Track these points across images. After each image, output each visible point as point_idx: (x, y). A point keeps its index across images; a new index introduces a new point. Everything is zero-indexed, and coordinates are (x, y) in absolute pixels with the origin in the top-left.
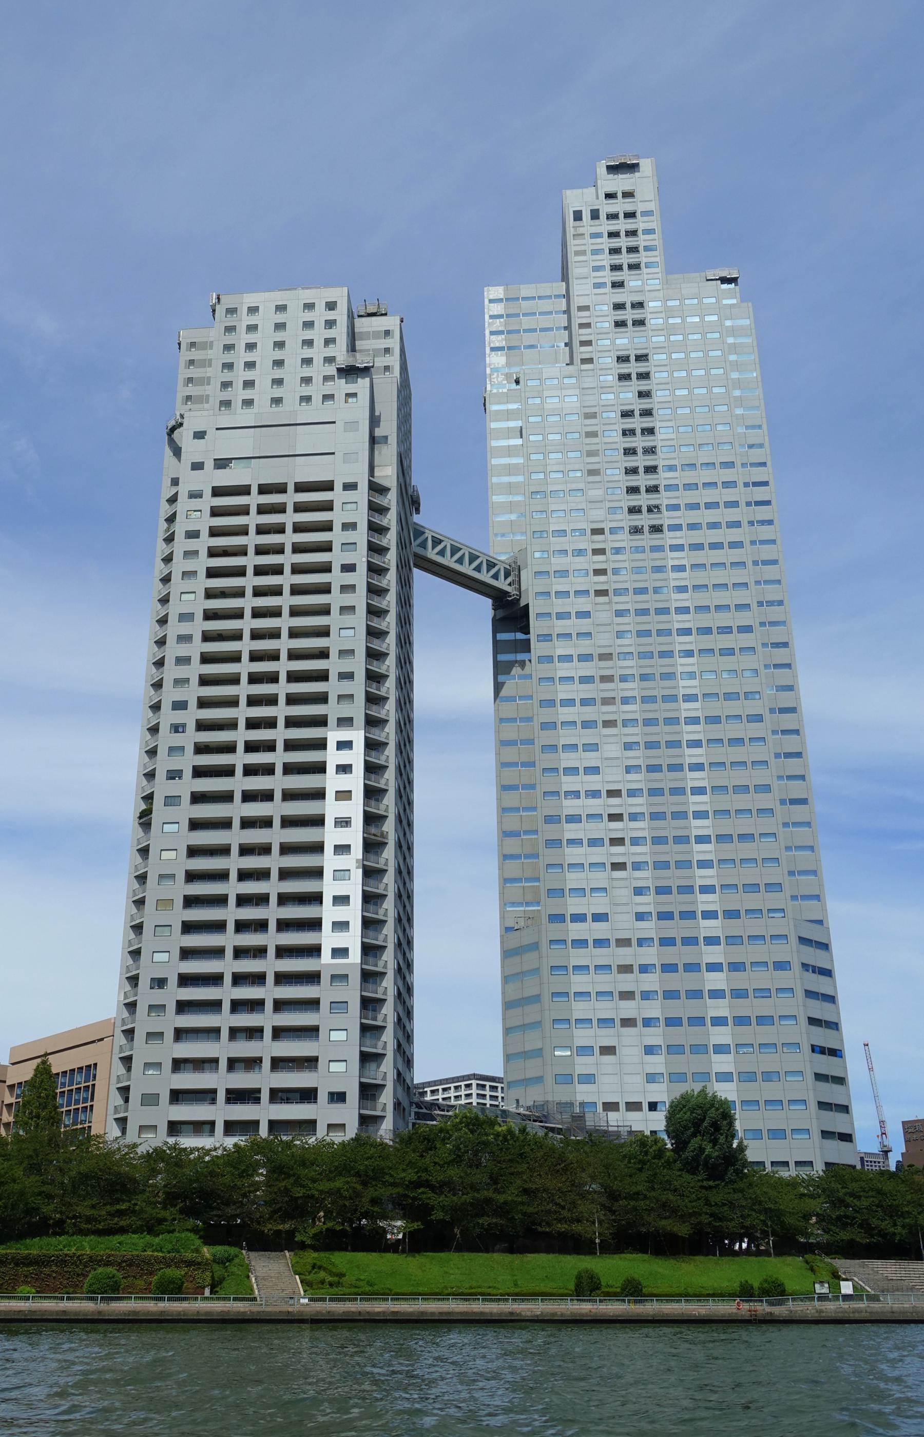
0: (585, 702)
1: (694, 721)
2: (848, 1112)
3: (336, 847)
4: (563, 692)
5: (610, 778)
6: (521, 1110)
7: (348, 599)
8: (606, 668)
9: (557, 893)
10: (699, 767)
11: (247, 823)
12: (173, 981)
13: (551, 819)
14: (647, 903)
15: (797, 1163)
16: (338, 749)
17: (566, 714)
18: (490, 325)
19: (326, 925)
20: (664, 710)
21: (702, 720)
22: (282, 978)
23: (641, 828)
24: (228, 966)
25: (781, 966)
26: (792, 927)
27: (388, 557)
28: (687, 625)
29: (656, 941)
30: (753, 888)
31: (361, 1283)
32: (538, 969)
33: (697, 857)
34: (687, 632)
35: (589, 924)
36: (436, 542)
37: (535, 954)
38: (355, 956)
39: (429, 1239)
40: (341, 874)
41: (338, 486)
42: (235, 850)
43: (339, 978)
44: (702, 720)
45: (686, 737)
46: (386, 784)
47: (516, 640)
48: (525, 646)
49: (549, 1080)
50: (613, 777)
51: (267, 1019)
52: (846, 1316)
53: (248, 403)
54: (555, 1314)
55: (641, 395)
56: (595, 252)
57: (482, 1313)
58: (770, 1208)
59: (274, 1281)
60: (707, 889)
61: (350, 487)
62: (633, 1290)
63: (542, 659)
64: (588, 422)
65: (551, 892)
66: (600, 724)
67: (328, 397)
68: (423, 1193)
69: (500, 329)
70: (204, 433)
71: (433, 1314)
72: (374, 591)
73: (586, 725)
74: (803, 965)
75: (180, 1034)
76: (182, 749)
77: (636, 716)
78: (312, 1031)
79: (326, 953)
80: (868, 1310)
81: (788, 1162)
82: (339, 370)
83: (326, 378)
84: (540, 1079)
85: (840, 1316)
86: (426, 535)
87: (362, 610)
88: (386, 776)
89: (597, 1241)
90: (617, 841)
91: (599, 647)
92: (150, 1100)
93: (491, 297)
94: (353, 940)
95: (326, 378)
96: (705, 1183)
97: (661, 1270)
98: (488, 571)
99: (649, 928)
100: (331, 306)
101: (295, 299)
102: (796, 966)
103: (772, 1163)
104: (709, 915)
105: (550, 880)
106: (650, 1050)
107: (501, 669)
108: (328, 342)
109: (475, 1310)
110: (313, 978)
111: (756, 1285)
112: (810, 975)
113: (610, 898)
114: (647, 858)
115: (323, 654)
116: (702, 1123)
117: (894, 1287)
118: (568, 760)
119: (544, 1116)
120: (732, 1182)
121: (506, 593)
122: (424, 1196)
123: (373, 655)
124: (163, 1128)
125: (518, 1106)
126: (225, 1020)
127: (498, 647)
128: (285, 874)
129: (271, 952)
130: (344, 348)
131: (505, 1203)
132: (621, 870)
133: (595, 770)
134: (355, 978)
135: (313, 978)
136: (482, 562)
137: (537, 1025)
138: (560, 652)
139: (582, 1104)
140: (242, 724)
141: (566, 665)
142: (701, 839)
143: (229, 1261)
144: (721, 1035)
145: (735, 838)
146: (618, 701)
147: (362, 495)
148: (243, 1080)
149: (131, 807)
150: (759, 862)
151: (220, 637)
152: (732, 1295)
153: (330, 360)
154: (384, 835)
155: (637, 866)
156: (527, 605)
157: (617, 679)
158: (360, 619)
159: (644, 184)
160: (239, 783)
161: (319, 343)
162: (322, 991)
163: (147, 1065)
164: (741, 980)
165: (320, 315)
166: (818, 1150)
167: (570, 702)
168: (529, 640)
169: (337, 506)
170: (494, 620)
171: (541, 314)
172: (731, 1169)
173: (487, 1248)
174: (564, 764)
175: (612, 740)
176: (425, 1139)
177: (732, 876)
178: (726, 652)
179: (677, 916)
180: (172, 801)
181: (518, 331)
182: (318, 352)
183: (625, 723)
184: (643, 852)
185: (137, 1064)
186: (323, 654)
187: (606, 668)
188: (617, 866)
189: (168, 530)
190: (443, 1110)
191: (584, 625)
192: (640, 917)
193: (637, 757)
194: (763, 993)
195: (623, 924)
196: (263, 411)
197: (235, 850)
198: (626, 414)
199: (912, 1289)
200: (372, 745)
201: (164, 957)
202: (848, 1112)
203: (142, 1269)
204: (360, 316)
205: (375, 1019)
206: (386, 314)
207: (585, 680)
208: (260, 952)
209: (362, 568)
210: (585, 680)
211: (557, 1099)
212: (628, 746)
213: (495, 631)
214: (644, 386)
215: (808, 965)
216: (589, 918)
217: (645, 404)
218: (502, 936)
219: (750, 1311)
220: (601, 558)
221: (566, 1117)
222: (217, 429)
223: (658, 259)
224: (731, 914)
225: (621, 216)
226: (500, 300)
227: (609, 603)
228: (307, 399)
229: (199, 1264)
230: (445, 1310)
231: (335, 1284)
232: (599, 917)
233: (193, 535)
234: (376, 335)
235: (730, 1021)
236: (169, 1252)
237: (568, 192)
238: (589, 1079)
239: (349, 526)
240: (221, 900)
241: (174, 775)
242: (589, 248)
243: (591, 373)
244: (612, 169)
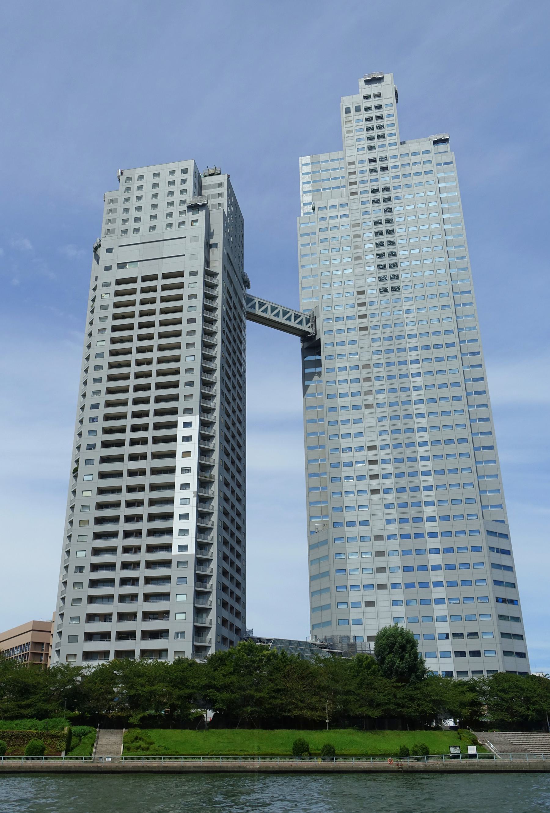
0: (354, 394)
1: (421, 402)
2: (522, 639)
3: (182, 485)
4: (341, 389)
5: (370, 439)
6: (318, 642)
7: (191, 339)
8: (366, 373)
9: (338, 509)
10: (424, 429)
11: (132, 473)
12: (88, 568)
13: (335, 465)
14: (392, 513)
15: (473, 672)
16: (184, 427)
17: (343, 402)
18: (303, 179)
19: (175, 532)
20: (402, 396)
21: (425, 401)
22: (150, 564)
23: (388, 468)
25: (476, 549)
26: (482, 524)
27: (217, 313)
28: (415, 345)
29: (399, 537)
30: (458, 501)
31: (161, 748)
32: (328, 555)
33: (423, 484)
34: (415, 349)
35: (358, 527)
36: (261, 305)
37: (326, 547)
38: (192, 550)
39: (226, 720)
40: (184, 501)
41: (186, 274)
42: (124, 489)
43: (182, 563)
44: (425, 401)
45: (415, 412)
46: (214, 447)
47: (315, 360)
48: (318, 363)
49: (334, 623)
50: (371, 438)
52: (464, 768)
53: (137, 230)
54: (269, 767)
55: (386, 211)
56: (358, 130)
57: (221, 767)
58: (437, 700)
59: (109, 747)
60: (429, 504)
62: (329, 752)
63: (328, 370)
64: (355, 229)
65: (335, 509)
66: (363, 407)
67: (181, 223)
68: (211, 692)
69: (309, 180)
70: (112, 249)
71: (190, 767)
72: (207, 333)
73: (355, 407)
74: (490, 548)
75: (92, 599)
76: (96, 431)
77: (385, 401)
78: (165, 596)
79: (175, 548)
80: (479, 764)
81: (482, 671)
82: (188, 207)
83: (181, 213)
84: (329, 623)
85: (459, 768)
86: (255, 301)
87: (199, 345)
88: (214, 442)
89: (327, 721)
90: (374, 477)
91: (362, 361)
92: (73, 639)
93: (303, 163)
94: (190, 540)
95: (181, 213)
96: (395, 684)
97: (358, 739)
98: (295, 320)
99: (394, 529)
100: (185, 171)
101: (164, 169)
102: (485, 549)
103: (487, 671)
104: (431, 519)
105: (335, 501)
106: (395, 603)
107: (307, 377)
108: (183, 192)
109: (217, 765)
110: (167, 563)
111: (410, 748)
112: (495, 554)
113: (371, 511)
114: (392, 486)
115: (177, 372)
116: (398, 648)
117: (514, 749)
118: (344, 429)
119: (331, 645)
120: (414, 683)
121: (307, 333)
122: (211, 694)
123: (206, 371)
124: (80, 656)
125: (316, 639)
126: (117, 590)
127: (305, 365)
128: (152, 502)
129: (144, 533)
130: (191, 194)
131: (260, 697)
132: (377, 494)
133: (360, 434)
134: (192, 563)
135: (167, 563)
136: (291, 315)
137: (328, 589)
138: (339, 365)
139: (355, 637)
141: (343, 373)
142: (425, 473)
143: (84, 735)
144: (439, 593)
145: (446, 472)
146: (374, 392)
147: (200, 278)
148: (126, 626)
149: (69, 467)
150: (461, 486)
151: (120, 365)
152: (395, 755)
153: (183, 202)
154: (211, 477)
155: (386, 491)
156: (320, 339)
157: (373, 379)
158: (198, 350)
159: (386, 89)
161: (177, 192)
162: (172, 572)
163: (72, 618)
164: (451, 559)
165: (178, 177)
166: (501, 664)
167: (345, 395)
168: (321, 360)
170: (303, 349)
171: (332, 170)
172: (413, 676)
173: (252, 726)
174: (342, 432)
175: (371, 416)
176: (219, 659)
177: (444, 494)
178: (438, 359)
179: (411, 520)
180: (89, 462)
181: (319, 181)
182: (177, 198)
183: (378, 405)
184: (390, 483)
185: (66, 617)
186: (177, 372)
187: (366, 373)
188: (374, 492)
189: (92, 306)
190: (264, 643)
191: (353, 348)
192: (389, 522)
193: (385, 425)
194: (465, 566)
195: (379, 526)
196: (145, 234)
197: (124, 489)
198: (377, 223)
199: (525, 750)
200: (204, 424)
202: (522, 639)
203: (24, 740)
204: (205, 176)
205: (205, 587)
206: (220, 174)
207: (354, 381)
208: (137, 549)
209: (199, 321)
210: (354, 381)
211: (339, 635)
212: (380, 419)
213: (304, 357)
214: (387, 205)
215: (494, 548)
216: (358, 524)
217: (388, 216)
218: (308, 537)
219: (398, 765)
220: (363, 308)
221: (345, 646)
222: (119, 246)
223: (395, 131)
224: (444, 518)
225: (373, 108)
226: (308, 164)
227: (368, 335)
228: (170, 225)
229: (59, 737)
230: (197, 765)
231: (148, 750)
232: (364, 523)
234: (214, 186)
235: (445, 584)
236: (41, 730)
237: (345, 98)
238: (358, 622)
239: (192, 297)
240: (116, 519)
242: (354, 129)
243: (356, 201)
244: (368, 82)
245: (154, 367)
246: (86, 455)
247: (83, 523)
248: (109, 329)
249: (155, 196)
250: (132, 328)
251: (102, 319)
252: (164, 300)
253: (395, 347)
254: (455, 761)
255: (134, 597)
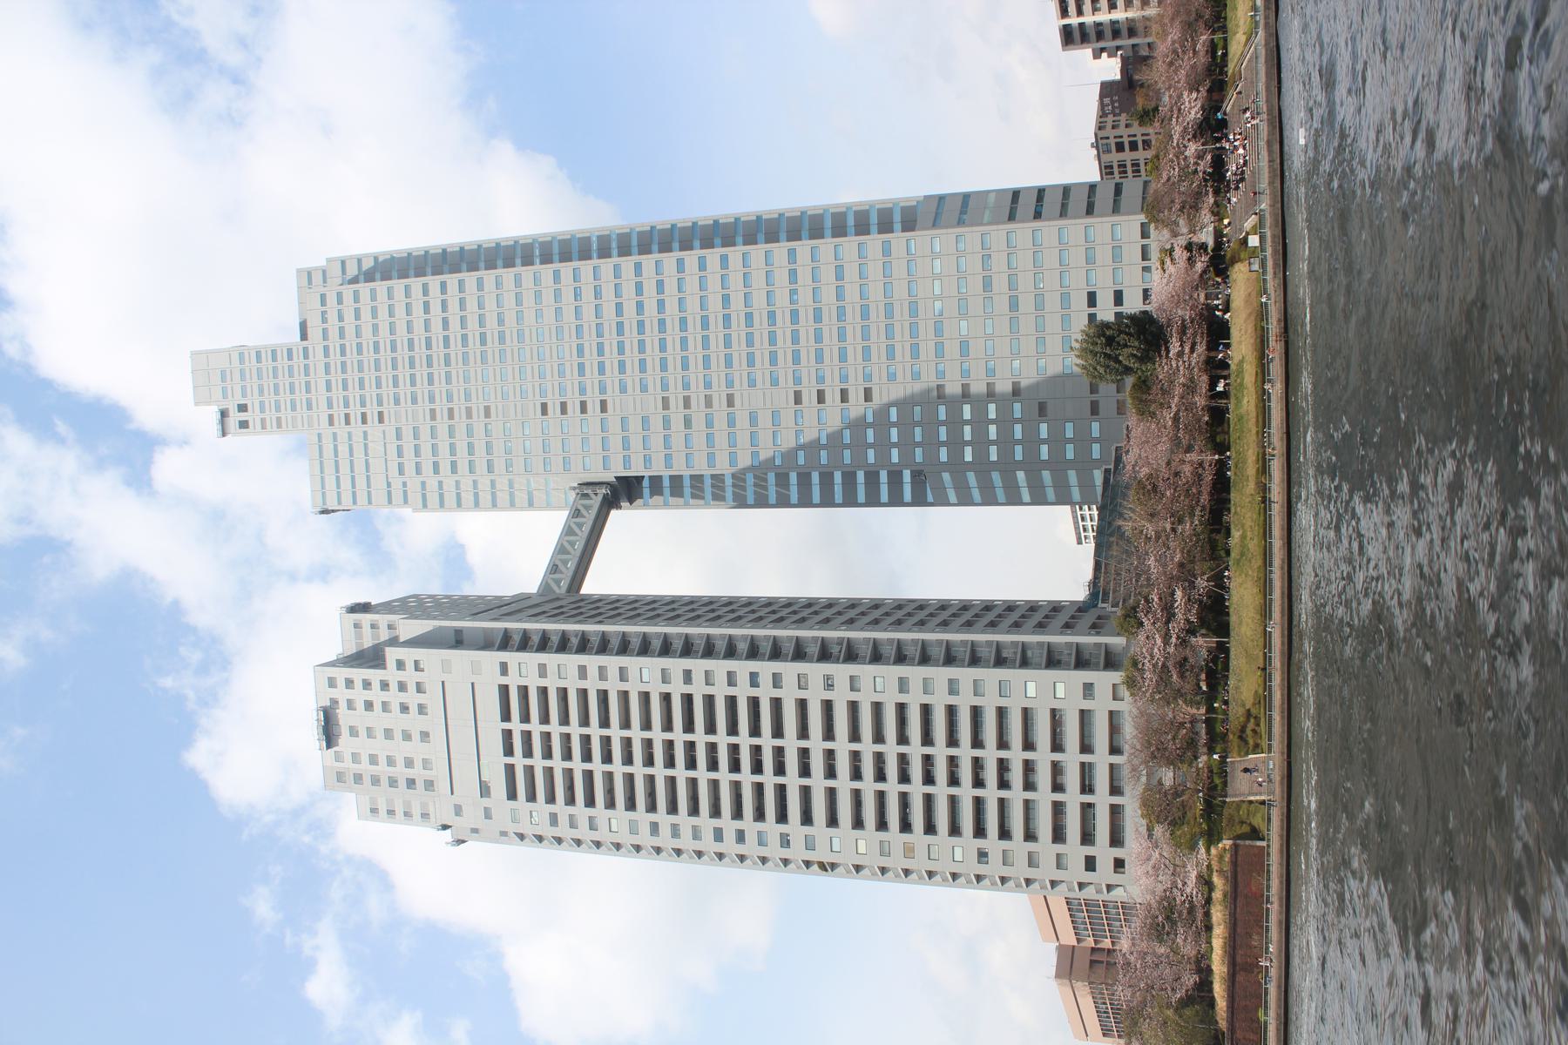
7: (613, 673)
12: (980, 843)
24: (917, 789)
41: (504, 681)
51: (990, 755)
61: (504, 668)
129: (928, 750)
140: (735, 777)
149: (817, 879)
160: (792, 780)
169: (562, 684)
180: (810, 844)
201: (958, 851)
233: (554, 819)
239: (583, 673)
241: (785, 841)
245: (658, 735)
246: (797, 852)
247: (909, 851)
248: (590, 811)
249: (370, 733)
250: (591, 772)
251: (573, 824)
252: (605, 723)
253: (678, 335)
254: (1270, 263)
255: (1029, 767)
